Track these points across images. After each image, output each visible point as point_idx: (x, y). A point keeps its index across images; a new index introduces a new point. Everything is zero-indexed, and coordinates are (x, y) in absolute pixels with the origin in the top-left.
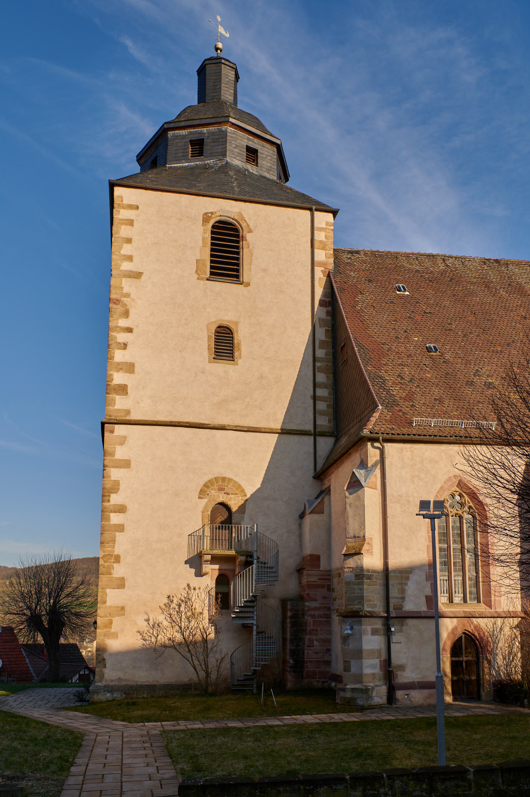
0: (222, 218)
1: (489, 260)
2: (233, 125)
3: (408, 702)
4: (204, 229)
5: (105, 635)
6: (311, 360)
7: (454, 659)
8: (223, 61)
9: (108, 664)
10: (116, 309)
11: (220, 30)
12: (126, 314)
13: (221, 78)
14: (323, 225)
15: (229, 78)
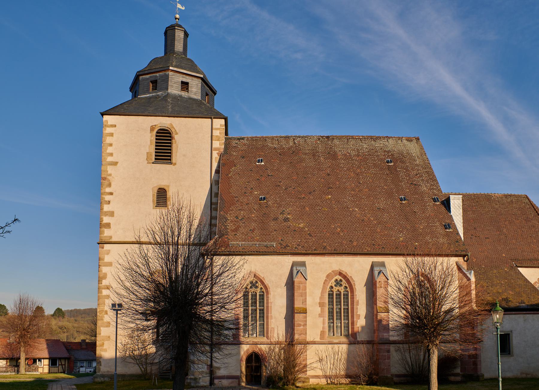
0: (162, 128)
1: (322, 137)
2: (172, 71)
6: (209, 204)
9: (102, 364)
10: (106, 183)
12: (110, 185)
14: (219, 127)
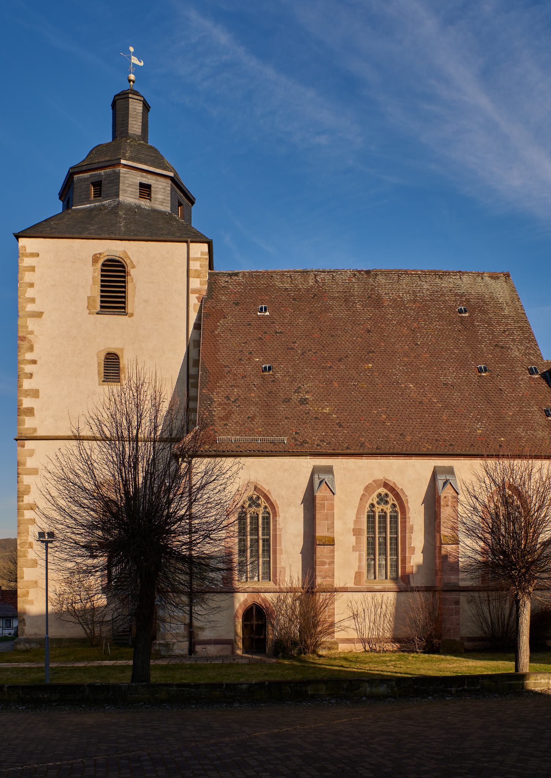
0: (110, 257)
1: (359, 272)
2: (125, 166)
3: (205, 654)
4: (94, 269)
5: (24, 602)
7: (246, 623)
8: (130, 96)
11: (133, 61)
12: (31, 349)
13: (128, 113)
14: (199, 255)
15: (137, 111)
